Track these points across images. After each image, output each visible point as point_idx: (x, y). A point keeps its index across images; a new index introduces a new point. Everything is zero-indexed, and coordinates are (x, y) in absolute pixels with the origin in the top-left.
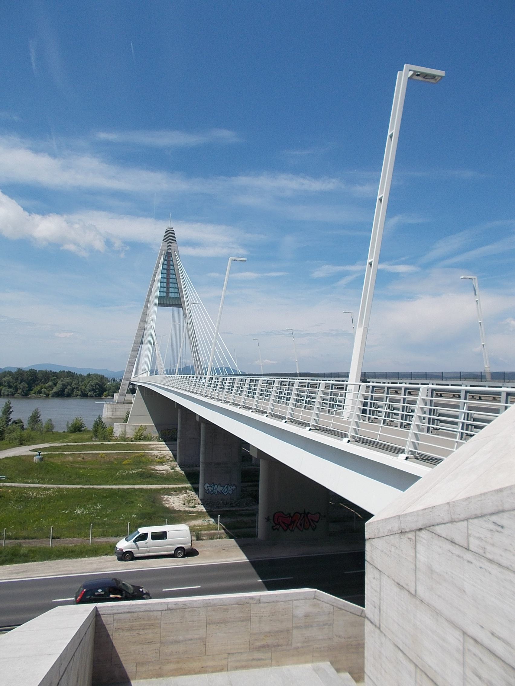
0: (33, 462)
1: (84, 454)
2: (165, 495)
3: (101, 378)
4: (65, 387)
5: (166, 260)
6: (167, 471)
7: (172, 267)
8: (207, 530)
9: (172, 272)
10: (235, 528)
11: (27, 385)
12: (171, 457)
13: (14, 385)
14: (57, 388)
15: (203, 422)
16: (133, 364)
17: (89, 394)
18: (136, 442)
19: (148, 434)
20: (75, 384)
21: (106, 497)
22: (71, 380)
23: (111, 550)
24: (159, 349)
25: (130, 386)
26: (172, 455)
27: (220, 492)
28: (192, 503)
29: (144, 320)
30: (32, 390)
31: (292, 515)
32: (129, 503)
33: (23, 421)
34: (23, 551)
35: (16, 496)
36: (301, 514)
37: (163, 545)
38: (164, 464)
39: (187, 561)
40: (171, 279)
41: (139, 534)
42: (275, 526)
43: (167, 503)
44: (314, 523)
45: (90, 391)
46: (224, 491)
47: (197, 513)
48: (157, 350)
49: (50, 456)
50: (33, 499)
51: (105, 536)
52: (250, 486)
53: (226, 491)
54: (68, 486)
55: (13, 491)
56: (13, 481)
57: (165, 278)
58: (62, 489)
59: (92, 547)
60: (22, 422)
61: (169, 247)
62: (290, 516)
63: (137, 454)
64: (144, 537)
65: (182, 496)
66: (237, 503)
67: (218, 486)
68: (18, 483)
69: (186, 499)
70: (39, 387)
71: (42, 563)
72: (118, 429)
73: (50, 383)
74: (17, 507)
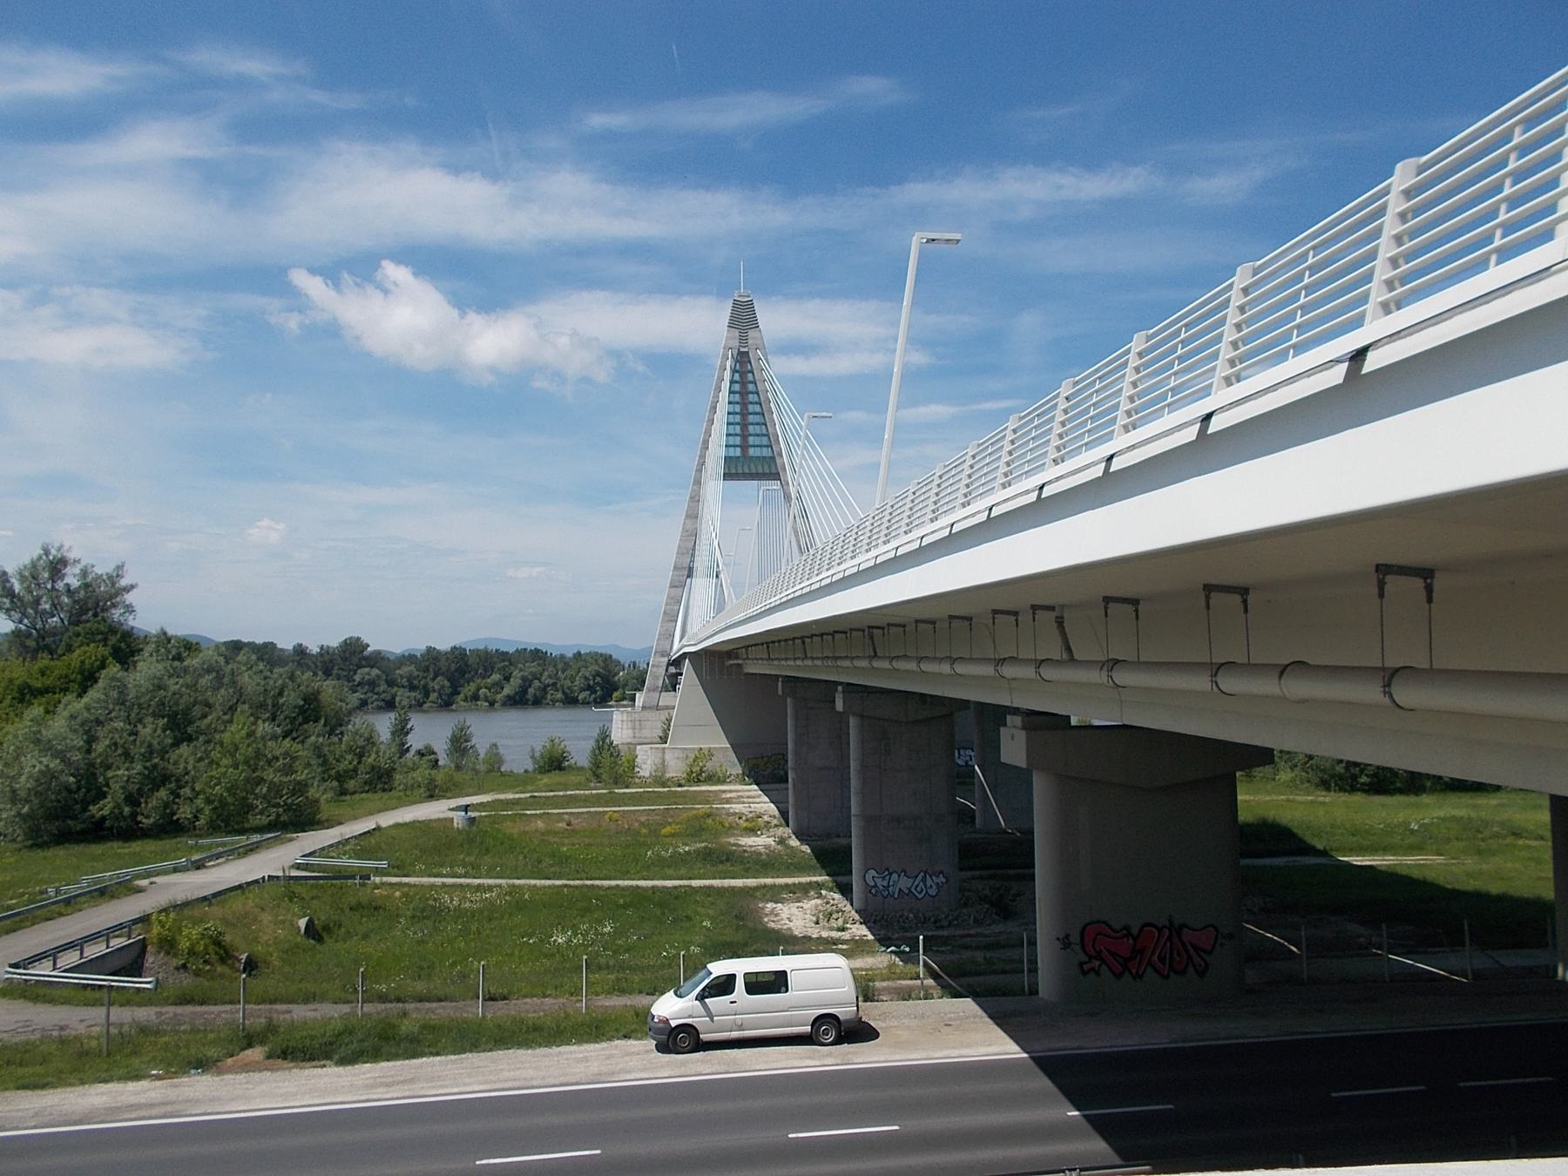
0: (453, 828)
1: (572, 813)
2: (767, 901)
3: (606, 659)
4: (527, 684)
5: (737, 372)
6: (767, 847)
7: (751, 387)
8: (888, 979)
9: (752, 397)
10: (964, 975)
11: (447, 683)
12: (775, 817)
13: (422, 683)
14: (511, 685)
15: (854, 714)
16: (673, 616)
17: (581, 697)
18: (690, 786)
19: (718, 769)
20: (550, 676)
21: (625, 907)
22: (540, 668)
23: (638, 1024)
24: (729, 581)
25: (670, 667)
26: (777, 813)
27: (907, 892)
28: (837, 920)
29: (693, 515)
30: (459, 694)
31: (1135, 931)
32: (682, 920)
33: (436, 750)
34: (407, 1027)
35: (411, 906)
36: (1160, 930)
37: (781, 1009)
38: (759, 833)
39: (850, 1053)
40: (751, 414)
41: (712, 977)
42: (1085, 963)
43: (775, 919)
44: (1202, 954)
45: (582, 690)
46: (916, 889)
47: (852, 943)
48: (726, 584)
49: (495, 820)
50: (452, 913)
51: (623, 992)
52: (981, 878)
53: (922, 890)
54: (533, 882)
55: (405, 895)
56: (405, 872)
57: (737, 413)
58: (519, 887)
59: (587, 1018)
60: (434, 753)
61: (743, 339)
62: (1129, 934)
63: (694, 812)
64: (724, 985)
65: (811, 904)
66: (950, 918)
67: (899, 876)
68: (418, 877)
69: (820, 911)
70: (473, 686)
71: (456, 1060)
72: (646, 762)
73: (496, 677)
74: (415, 933)
